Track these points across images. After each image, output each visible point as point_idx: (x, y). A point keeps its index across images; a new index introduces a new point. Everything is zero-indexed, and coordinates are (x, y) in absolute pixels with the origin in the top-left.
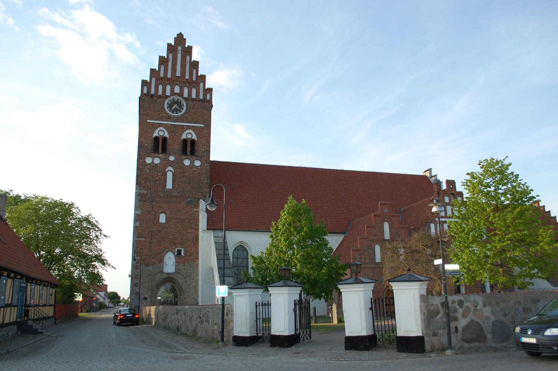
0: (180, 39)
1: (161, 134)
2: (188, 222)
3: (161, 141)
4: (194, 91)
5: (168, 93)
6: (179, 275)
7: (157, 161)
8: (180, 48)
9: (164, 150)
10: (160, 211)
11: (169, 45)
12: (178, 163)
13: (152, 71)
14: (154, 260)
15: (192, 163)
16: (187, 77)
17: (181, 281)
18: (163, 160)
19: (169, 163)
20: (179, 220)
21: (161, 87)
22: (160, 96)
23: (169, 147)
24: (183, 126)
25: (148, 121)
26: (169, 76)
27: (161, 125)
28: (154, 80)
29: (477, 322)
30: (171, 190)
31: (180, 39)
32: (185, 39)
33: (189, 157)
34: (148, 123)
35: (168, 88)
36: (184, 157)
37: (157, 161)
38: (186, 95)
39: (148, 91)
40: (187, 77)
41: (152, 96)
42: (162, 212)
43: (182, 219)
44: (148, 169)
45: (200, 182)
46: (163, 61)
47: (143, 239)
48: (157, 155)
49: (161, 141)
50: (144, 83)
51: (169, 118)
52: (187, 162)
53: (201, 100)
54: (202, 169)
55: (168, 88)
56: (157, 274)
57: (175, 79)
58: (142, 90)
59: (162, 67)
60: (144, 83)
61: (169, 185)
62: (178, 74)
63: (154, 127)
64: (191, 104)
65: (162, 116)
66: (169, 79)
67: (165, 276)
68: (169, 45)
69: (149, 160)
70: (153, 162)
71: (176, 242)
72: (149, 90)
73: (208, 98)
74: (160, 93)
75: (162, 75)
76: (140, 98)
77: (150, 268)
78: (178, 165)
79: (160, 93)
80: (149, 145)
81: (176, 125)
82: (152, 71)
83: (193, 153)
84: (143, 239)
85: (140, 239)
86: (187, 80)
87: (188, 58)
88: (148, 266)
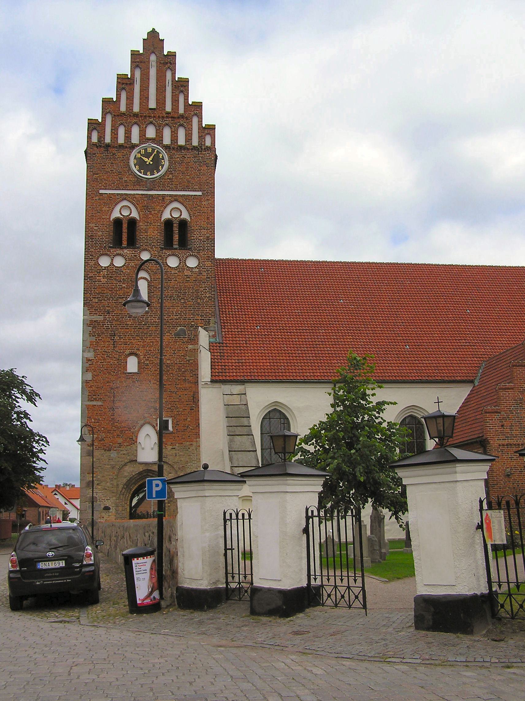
3: (125, 226)
5: (135, 139)
7: (119, 262)
8: (153, 58)
9: (132, 242)
10: (127, 352)
13: (106, 102)
14: (120, 441)
21: (121, 131)
23: (141, 236)
28: (109, 119)
29: (140, 485)
33: (177, 252)
35: (135, 131)
37: (119, 262)
38: (167, 141)
40: (169, 108)
46: (124, 83)
47: (100, 403)
48: (119, 251)
50: (93, 125)
51: (139, 183)
52: (173, 262)
55: (135, 131)
56: (125, 465)
58: (89, 137)
59: (124, 95)
60: (93, 125)
62: (152, 104)
63: (113, 200)
64: (177, 156)
65: (126, 181)
67: (141, 468)
68: (134, 54)
70: (112, 264)
72: (101, 137)
73: (208, 143)
74: (121, 140)
77: (113, 454)
79: (121, 140)
80: (105, 234)
82: (106, 102)
83: (184, 243)
84: (100, 403)
85: (95, 403)
87: (169, 74)
88: (110, 450)
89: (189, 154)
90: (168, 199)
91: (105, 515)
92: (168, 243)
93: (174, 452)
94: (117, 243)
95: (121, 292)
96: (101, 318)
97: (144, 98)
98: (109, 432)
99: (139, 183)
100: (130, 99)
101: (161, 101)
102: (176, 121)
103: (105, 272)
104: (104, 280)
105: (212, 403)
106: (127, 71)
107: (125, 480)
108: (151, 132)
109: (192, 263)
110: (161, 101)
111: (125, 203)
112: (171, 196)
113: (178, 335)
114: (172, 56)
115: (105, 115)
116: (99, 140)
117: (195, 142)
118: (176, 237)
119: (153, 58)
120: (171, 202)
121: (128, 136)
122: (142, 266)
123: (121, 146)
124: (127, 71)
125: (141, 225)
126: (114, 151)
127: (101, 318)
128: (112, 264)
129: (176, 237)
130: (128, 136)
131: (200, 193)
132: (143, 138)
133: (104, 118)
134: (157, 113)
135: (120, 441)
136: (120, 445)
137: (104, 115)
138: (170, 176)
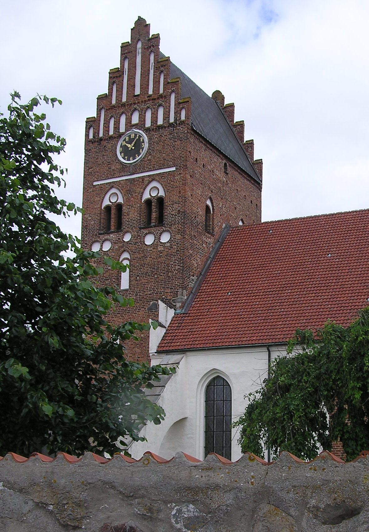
0: (141, 27)
15: (20, 175)
18: (115, 243)
22: (111, 138)
24: (143, 178)
41: (101, 139)
49: (113, 212)
63: (104, 190)
64: (156, 135)
65: (114, 170)
66: (124, 105)
70: (101, 249)
72: (96, 133)
81: (133, 179)
83: (161, 220)
86: (150, 96)
97: (131, 86)
112: (149, 176)
114: (157, 38)
121: (117, 127)
130: (117, 127)
133: (110, 89)
137: (99, 111)
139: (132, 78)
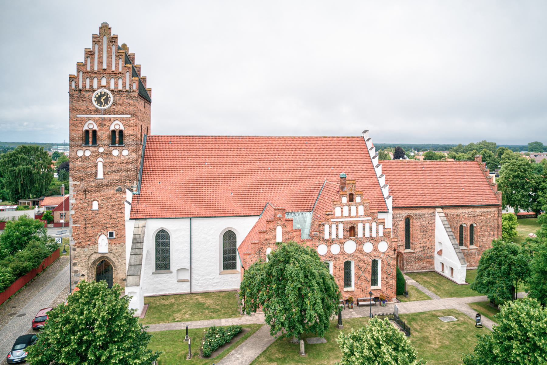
0: (105, 29)
1: (91, 127)
2: (118, 207)
3: (91, 134)
4: (120, 82)
5: (95, 86)
6: (112, 254)
7: (88, 153)
8: (105, 39)
9: (95, 142)
10: (92, 200)
11: (94, 37)
12: (107, 154)
13: (79, 65)
14: (89, 243)
16: (113, 68)
17: (114, 259)
19: (99, 155)
20: (110, 207)
21: (88, 81)
23: (99, 139)
24: (110, 118)
25: (78, 116)
26: (96, 69)
27: (90, 119)
28: (81, 74)
30: (102, 179)
31: (105, 29)
32: (110, 29)
33: (117, 148)
34: (77, 117)
35: (96, 81)
36: (113, 148)
37: (88, 153)
38: (112, 87)
39: (76, 86)
40: (113, 68)
42: (94, 200)
43: (112, 206)
44: (80, 161)
45: (127, 171)
46: (89, 54)
47: (79, 225)
48: (87, 148)
49: (91, 134)
50: (72, 78)
51: (97, 111)
52: (115, 153)
53: (127, 91)
54: (129, 159)
55: (96, 81)
56: (92, 254)
57: (101, 71)
58: (70, 86)
59: (89, 60)
60: (72, 78)
61: (100, 175)
62: (105, 66)
63: (83, 121)
64: (118, 96)
65: (90, 110)
67: (100, 256)
68: (94, 37)
69: (80, 153)
70: (84, 155)
71: (108, 226)
74: (88, 87)
75: (89, 69)
76: (145, 95)
77: (86, 250)
78: (107, 156)
79: (88, 87)
80: (79, 138)
82: (79, 65)
83: (121, 142)
84: (79, 225)
85: (76, 225)
88: (84, 248)
89: (124, 95)
90: (112, 120)
91: (83, 273)
92: (113, 143)
93: (115, 247)
94: (86, 142)
95: (89, 169)
96: (79, 183)
97: (100, 63)
98: (84, 239)
99: (97, 111)
100: (92, 63)
101: (109, 65)
102: (117, 75)
103: (80, 159)
104: (80, 163)
105: (130, 229)
106: (75, 73)
107: (92, 261)
108: (104, 82)
109: (125, 153)
110: (109, 65)
111: (91, 122)
112: (114, 118)
113: (117, 190)
115: (79, 72)
116: (76, 88)
117: (127, 88)
118: (117, 139)
119: (105, 39)
120: (114, 121)
121: (91, 86)
122: (100, 155)
123: (88, 91)
124: (75, 73)
125: (99, 134)
126: (84, 93)
127: (79, 183)
128: (84, 155)
129: (117, 139)
130: (91, 86)
131: (130, 116)
132: (100, 86)
133: (86, 61)
134: (107, 72)
135: (89, 243)
136: (89, 245)
137: (78, 72)
138: (114, 107)
139: (100, 57)
